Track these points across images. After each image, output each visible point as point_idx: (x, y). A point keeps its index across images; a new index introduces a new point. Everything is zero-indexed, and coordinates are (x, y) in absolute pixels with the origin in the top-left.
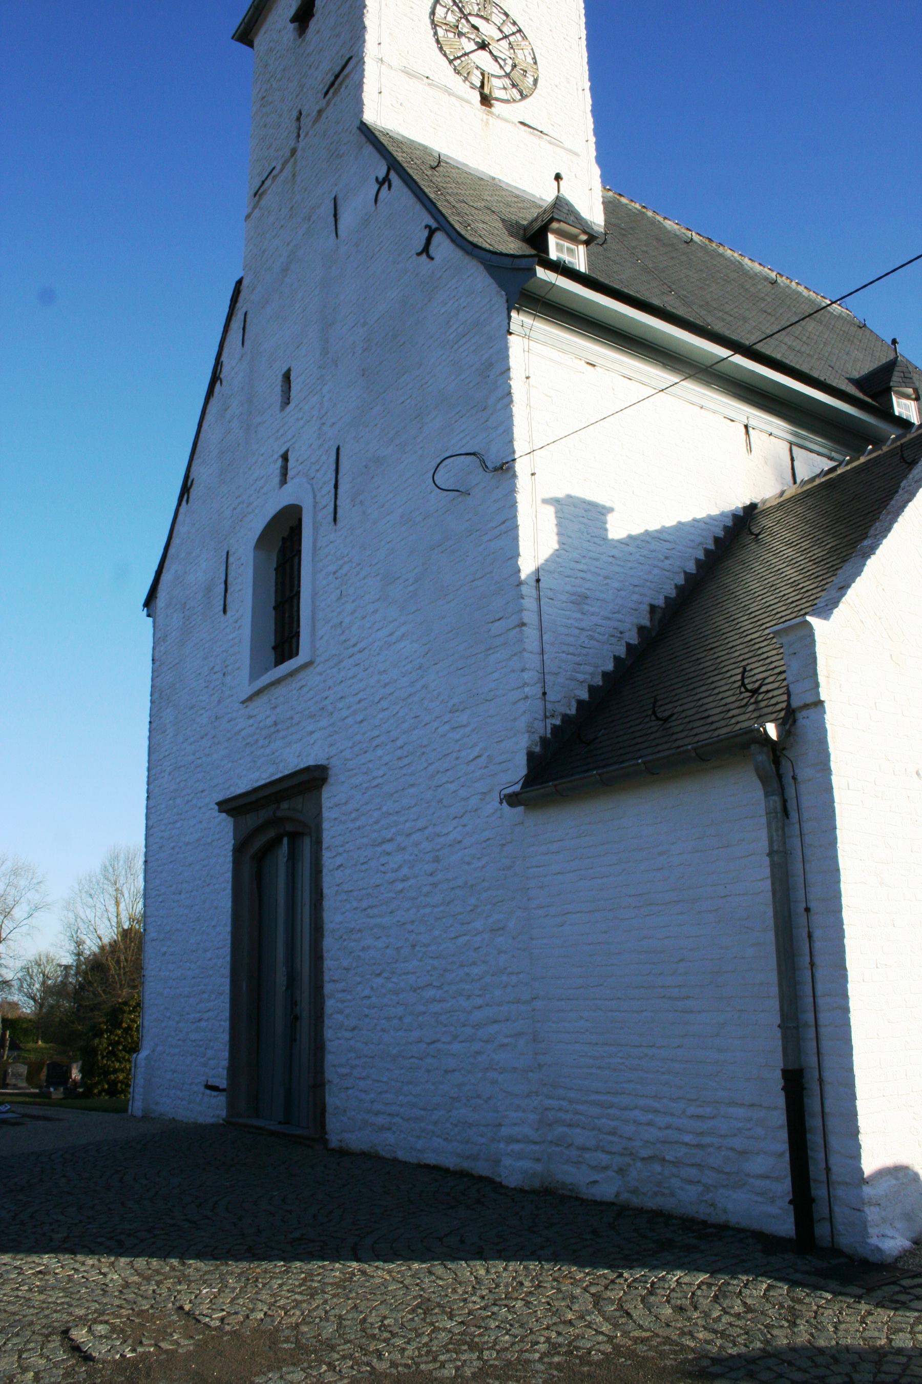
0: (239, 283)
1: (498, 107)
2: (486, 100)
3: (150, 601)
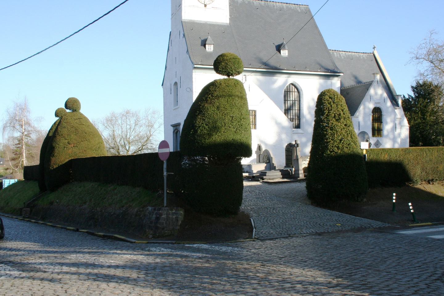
0: (170, 32)
1: (208, 6)
2: (205, 6)
3: (162, 85)
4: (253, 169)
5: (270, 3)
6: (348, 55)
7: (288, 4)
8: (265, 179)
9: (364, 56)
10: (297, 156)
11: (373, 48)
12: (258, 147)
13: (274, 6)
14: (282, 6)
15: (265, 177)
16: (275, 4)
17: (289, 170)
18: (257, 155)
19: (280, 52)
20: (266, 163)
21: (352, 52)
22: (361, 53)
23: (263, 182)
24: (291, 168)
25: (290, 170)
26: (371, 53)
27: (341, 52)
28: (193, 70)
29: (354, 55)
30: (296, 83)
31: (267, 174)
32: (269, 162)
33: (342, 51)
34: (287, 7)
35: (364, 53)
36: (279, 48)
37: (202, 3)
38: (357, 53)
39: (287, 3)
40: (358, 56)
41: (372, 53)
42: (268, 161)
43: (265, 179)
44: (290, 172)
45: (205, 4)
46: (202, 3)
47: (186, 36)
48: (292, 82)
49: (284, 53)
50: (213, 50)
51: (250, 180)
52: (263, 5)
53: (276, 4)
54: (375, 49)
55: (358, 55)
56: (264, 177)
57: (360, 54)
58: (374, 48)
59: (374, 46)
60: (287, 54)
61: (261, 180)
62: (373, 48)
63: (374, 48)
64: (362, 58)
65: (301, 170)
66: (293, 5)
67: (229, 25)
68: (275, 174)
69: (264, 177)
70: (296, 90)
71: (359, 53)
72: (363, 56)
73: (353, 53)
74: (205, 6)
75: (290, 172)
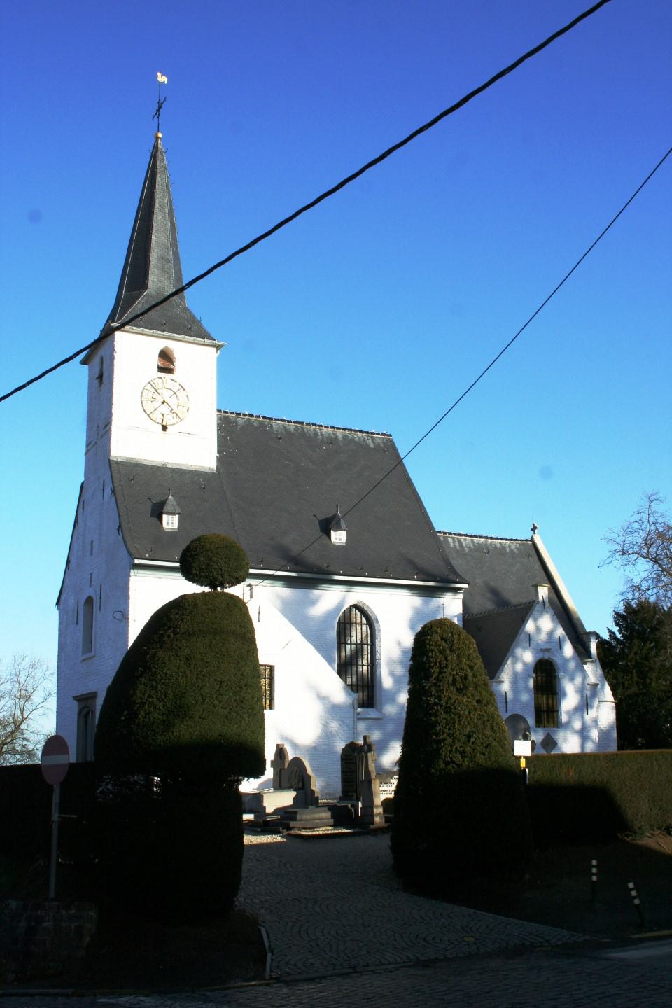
0: (83, 484)
1: (170, 429)
2: (164, 428)
3: (58, 603)
4: (265, 804)
5: (308, 427)
6: (478, 544)
7: (347, 432)
8: (293, 828)
9: (513, 547)
10: (368, 773)
11: (532, 530)
12: (277, 752)
13: (316, 434)
14: (333, 434)
15: (294, 822)
16: (318, 430)
17: (349, 806)
18: (274, 769)
19: (329, 536)
20: (294, 790)
21: (487, 538)
22: (506, 540)
23: (289, 835)
24: (355, 802)
25: (352, 806)
26: (527, 540)
27: (464, 537)
28: (132, 571)
29: (491, 544)
30: (364, 604)
31: (298, 817)
32: (303, 788)
33: (466, 535)
34: (345, 437)
35: (512, 540)
36: (327, 526)
37: (158, 423)
38: (497, 539)
39: (345, 429)
40: (499, 546)
41: (530, 541)
42: (300, 785)
43: (293, 828)
44: (353, 810)
45: (164, 424)
46: (158, 423)
47: (117, 493)
48: (356, 603)
49: (339, 537)
50: (179, 528)
51: (259, 830)
52: (293, 431)
53: (320, 429)
54: (536, 531)
55: (500, 543)
56: (292, 824)
57: (504, 541)
58: (534, 529)
59: (534, 524)
60: (344, 540)
61: (284, 830)
62: (532, 530)
63: (534, 529)
64: (508, 550)
65: (377, 806)
66: (358, 433)
67: (215, 472)
68: (317, 816)
69: (292, 824)
70: (364, 621)
71: (502, 539)
72: (510, 546)
73: (489, 541)
74: (164, 428)
75: (353, 810)
